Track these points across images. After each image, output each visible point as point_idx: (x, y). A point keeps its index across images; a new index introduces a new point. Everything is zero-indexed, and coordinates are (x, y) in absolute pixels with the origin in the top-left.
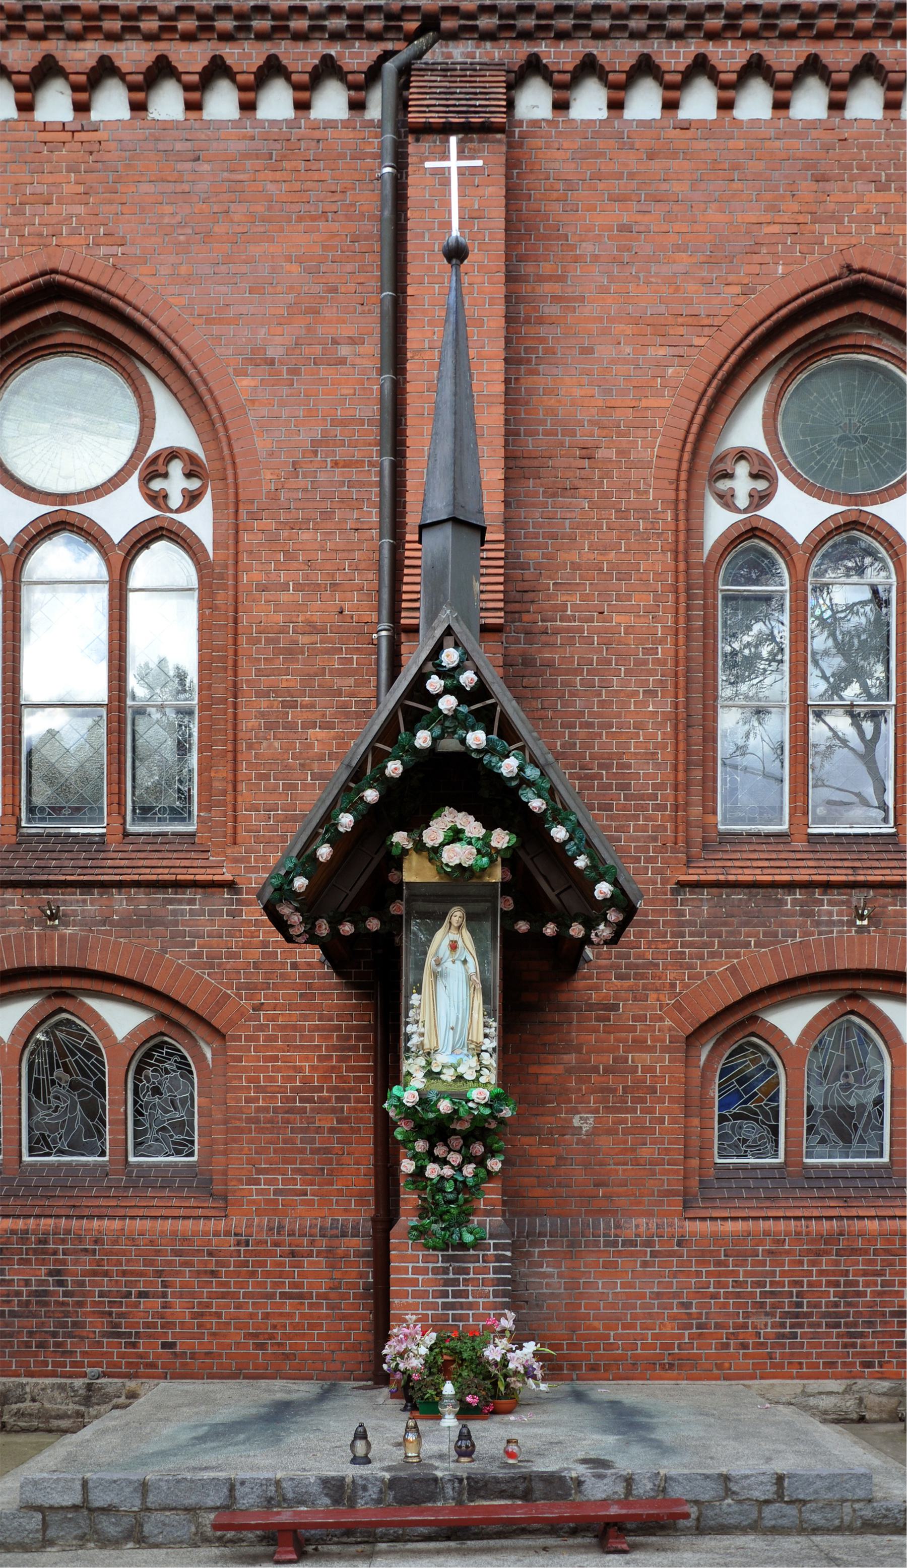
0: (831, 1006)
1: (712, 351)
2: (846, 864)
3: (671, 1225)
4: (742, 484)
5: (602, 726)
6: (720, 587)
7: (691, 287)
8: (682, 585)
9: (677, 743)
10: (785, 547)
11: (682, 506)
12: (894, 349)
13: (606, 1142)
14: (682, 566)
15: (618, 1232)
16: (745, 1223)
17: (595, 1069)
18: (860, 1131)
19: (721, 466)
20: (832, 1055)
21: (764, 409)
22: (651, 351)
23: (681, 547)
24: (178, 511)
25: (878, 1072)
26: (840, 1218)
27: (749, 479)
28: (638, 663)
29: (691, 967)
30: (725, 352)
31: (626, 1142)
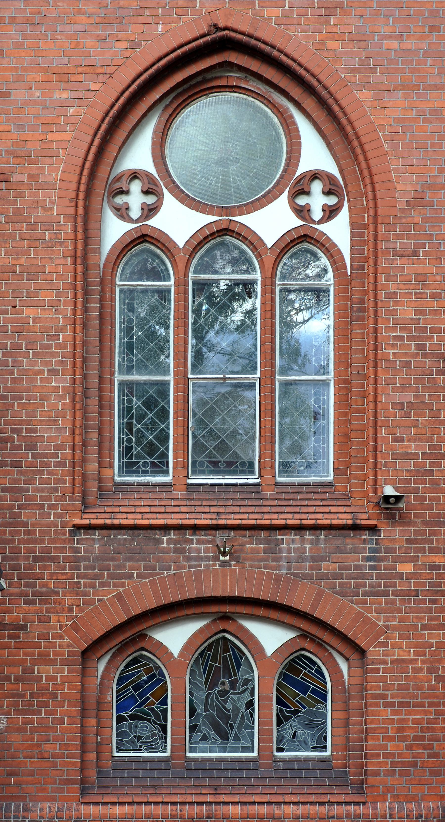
0: (207, 626)
1: (105, 94)
3: (69, 809)
5: (14, 398)
6: (118, 283)
7: (89, 43)
8: (79, 283)
9: (74, 412)
11: (79, 220)
12: (259, 89)
13: (17, 739)
14: (80, 268)
15: (26, 814)
16: (130, 807)
17: (8, 679)
18: (235, 730)
19: (117, 185)
20: (211, 666)
21: (153, 138)
22: (57, 95)
23: (79, 253)
24: (320, 222)
25: (250, 680)
26: (209, 803)
27: (142, 195)
28: (44, 347)
29: (85, 594)
30: (116, 94)
31: (33, 739)
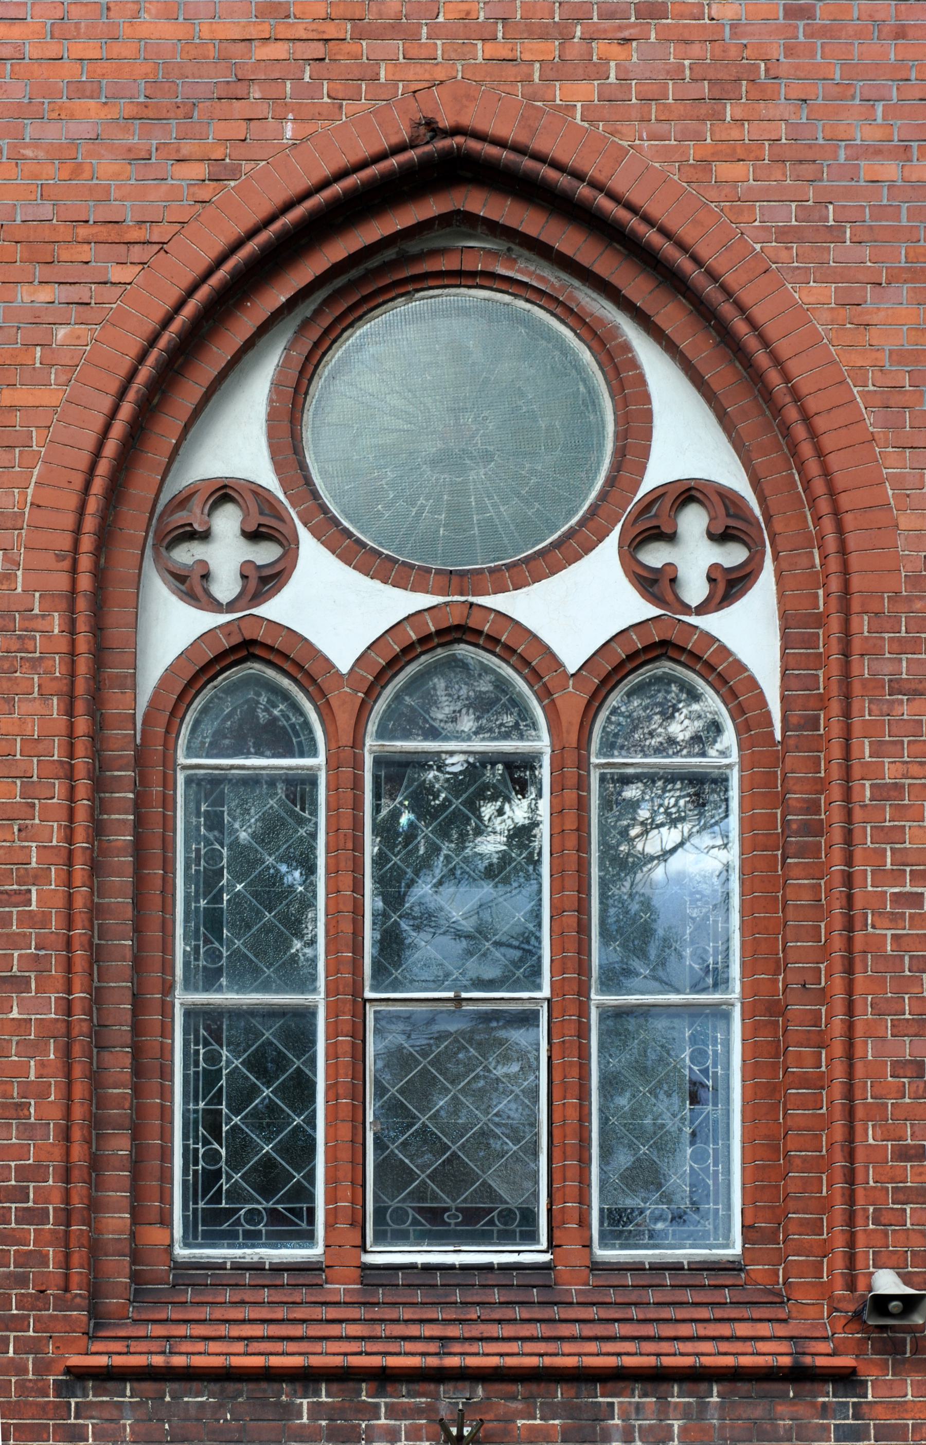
1: (148, 294)
2: (429, 1330)
4: (226, 552)
6: (182, 760)
7: (106, 167)
8: (81, 763)
9: (69, 1085)
10: (314, 681)
11: (82, 604)
12: (542, 279)
14: (82, 725)
19: (180, 517)
21: (271, 401)
22: (23, 295)
23: (81, 687)
24: (701, 610)
30: (175, 293)
